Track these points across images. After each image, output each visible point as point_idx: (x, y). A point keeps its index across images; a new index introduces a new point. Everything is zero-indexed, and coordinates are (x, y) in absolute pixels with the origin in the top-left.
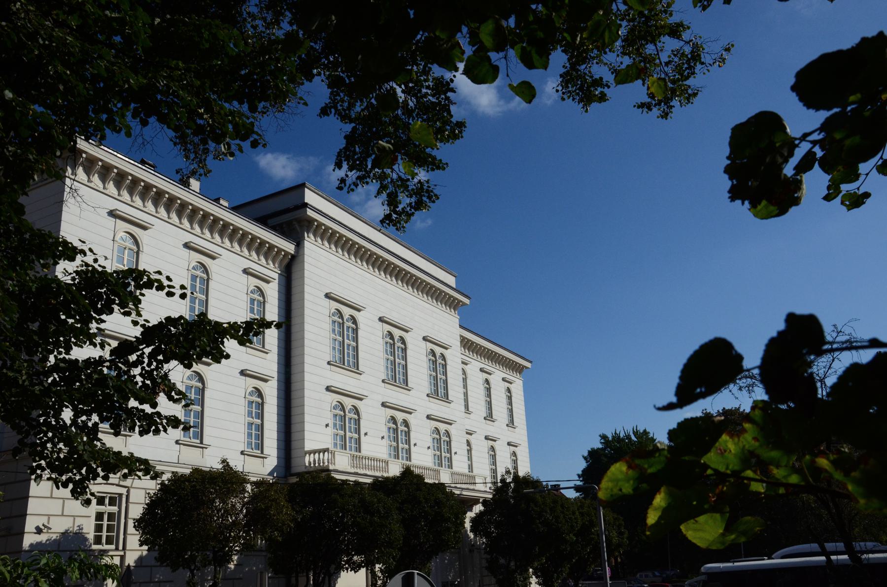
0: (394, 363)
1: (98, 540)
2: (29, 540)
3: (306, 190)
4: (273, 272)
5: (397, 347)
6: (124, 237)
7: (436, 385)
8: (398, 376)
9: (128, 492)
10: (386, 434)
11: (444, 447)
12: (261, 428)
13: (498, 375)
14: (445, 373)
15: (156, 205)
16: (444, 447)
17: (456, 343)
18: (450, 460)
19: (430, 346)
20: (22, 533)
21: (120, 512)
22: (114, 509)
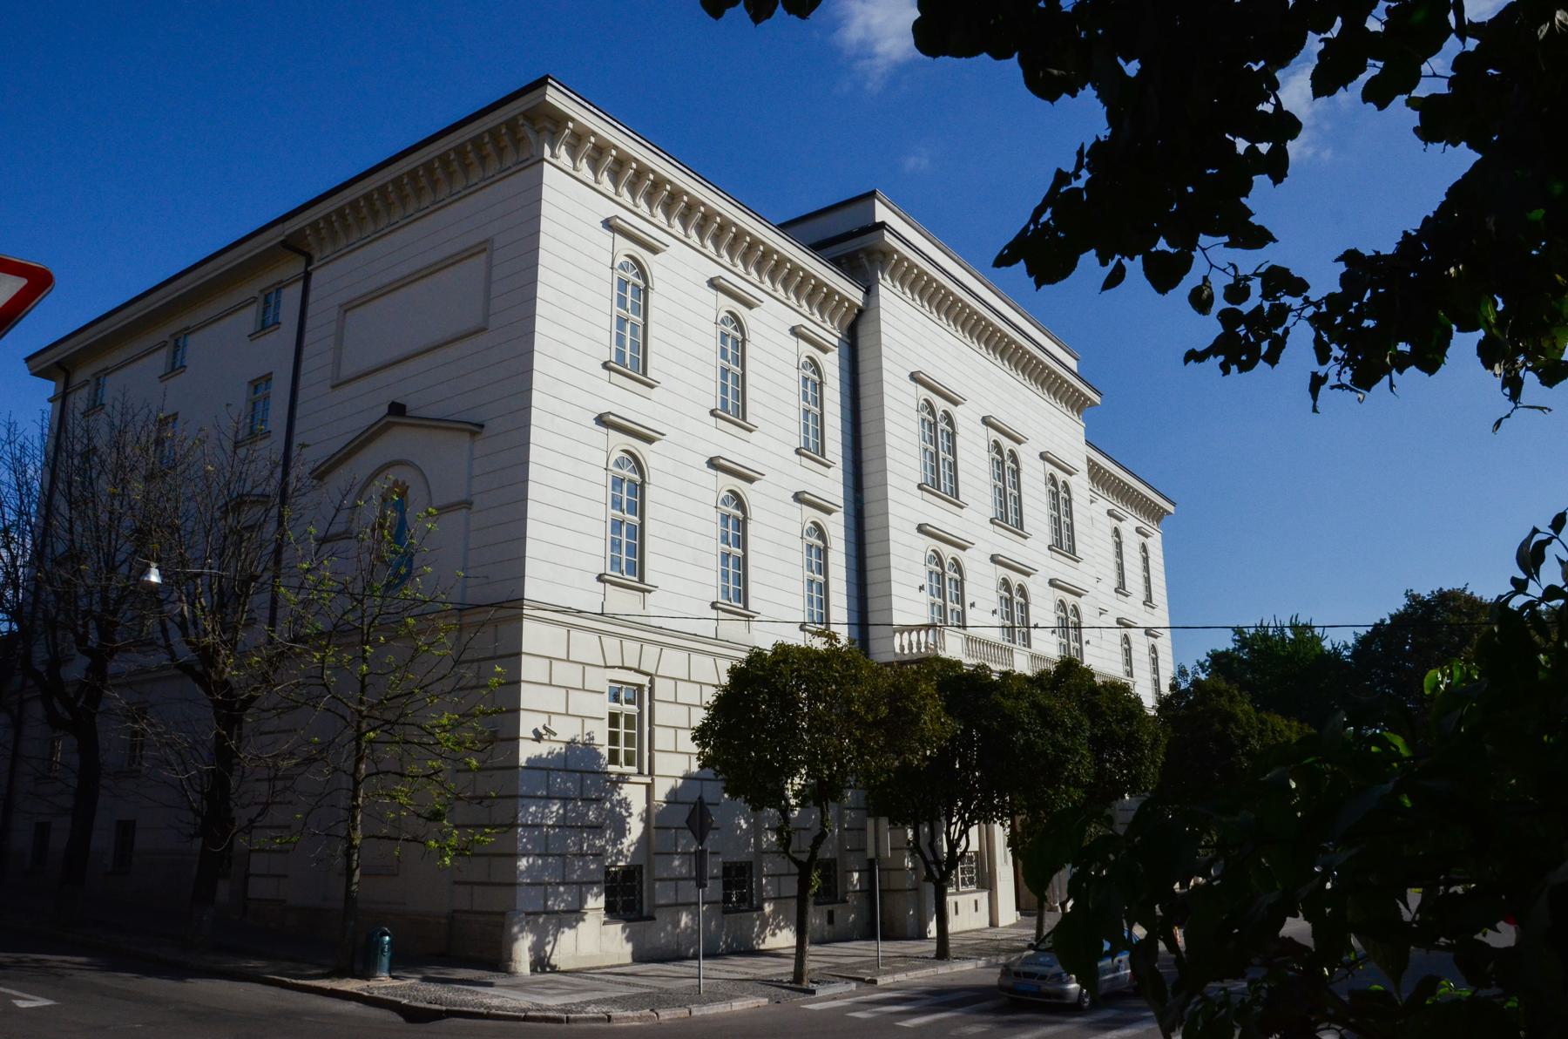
0: (935, 457)
1: (614, 757)
2: (528, 751)
4: (831, 334)
5: (1006, 467)
7: (936, 470)
8: (1009, 516)
9: (652, 682)
10: (996, 606)
11: (950, 590)
12: (824, 588)
14: (953, 450)
15: (595, 166)
16: (950, 590)
17: (1083, 467)
18: (962, 616)
19: (1050, 468)
20: (514, 739)
21: (641, 714)
22: (633, 709)
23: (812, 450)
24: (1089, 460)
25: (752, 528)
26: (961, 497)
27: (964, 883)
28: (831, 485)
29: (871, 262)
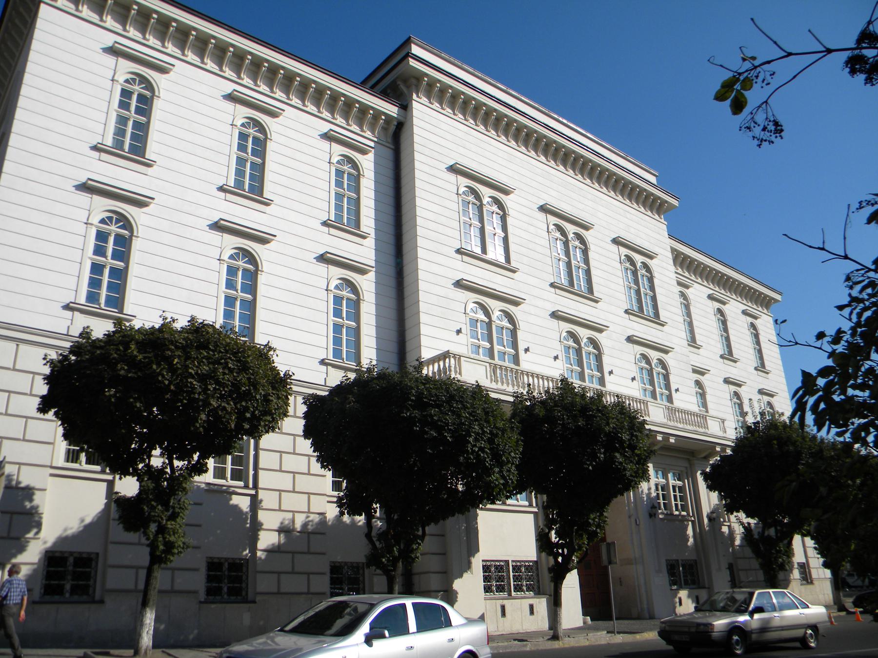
3: (413, 46)
6: (474, 309)
11: (659, 381)
13: (734, 307)
23: (345, 221)
24: (673, 250)
25: (262, 279)
26: (596, 294)
27: (516, 590)
28: (364, 251)
29: (408, 87)
